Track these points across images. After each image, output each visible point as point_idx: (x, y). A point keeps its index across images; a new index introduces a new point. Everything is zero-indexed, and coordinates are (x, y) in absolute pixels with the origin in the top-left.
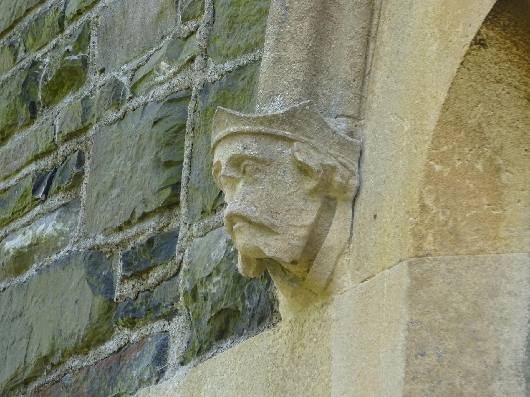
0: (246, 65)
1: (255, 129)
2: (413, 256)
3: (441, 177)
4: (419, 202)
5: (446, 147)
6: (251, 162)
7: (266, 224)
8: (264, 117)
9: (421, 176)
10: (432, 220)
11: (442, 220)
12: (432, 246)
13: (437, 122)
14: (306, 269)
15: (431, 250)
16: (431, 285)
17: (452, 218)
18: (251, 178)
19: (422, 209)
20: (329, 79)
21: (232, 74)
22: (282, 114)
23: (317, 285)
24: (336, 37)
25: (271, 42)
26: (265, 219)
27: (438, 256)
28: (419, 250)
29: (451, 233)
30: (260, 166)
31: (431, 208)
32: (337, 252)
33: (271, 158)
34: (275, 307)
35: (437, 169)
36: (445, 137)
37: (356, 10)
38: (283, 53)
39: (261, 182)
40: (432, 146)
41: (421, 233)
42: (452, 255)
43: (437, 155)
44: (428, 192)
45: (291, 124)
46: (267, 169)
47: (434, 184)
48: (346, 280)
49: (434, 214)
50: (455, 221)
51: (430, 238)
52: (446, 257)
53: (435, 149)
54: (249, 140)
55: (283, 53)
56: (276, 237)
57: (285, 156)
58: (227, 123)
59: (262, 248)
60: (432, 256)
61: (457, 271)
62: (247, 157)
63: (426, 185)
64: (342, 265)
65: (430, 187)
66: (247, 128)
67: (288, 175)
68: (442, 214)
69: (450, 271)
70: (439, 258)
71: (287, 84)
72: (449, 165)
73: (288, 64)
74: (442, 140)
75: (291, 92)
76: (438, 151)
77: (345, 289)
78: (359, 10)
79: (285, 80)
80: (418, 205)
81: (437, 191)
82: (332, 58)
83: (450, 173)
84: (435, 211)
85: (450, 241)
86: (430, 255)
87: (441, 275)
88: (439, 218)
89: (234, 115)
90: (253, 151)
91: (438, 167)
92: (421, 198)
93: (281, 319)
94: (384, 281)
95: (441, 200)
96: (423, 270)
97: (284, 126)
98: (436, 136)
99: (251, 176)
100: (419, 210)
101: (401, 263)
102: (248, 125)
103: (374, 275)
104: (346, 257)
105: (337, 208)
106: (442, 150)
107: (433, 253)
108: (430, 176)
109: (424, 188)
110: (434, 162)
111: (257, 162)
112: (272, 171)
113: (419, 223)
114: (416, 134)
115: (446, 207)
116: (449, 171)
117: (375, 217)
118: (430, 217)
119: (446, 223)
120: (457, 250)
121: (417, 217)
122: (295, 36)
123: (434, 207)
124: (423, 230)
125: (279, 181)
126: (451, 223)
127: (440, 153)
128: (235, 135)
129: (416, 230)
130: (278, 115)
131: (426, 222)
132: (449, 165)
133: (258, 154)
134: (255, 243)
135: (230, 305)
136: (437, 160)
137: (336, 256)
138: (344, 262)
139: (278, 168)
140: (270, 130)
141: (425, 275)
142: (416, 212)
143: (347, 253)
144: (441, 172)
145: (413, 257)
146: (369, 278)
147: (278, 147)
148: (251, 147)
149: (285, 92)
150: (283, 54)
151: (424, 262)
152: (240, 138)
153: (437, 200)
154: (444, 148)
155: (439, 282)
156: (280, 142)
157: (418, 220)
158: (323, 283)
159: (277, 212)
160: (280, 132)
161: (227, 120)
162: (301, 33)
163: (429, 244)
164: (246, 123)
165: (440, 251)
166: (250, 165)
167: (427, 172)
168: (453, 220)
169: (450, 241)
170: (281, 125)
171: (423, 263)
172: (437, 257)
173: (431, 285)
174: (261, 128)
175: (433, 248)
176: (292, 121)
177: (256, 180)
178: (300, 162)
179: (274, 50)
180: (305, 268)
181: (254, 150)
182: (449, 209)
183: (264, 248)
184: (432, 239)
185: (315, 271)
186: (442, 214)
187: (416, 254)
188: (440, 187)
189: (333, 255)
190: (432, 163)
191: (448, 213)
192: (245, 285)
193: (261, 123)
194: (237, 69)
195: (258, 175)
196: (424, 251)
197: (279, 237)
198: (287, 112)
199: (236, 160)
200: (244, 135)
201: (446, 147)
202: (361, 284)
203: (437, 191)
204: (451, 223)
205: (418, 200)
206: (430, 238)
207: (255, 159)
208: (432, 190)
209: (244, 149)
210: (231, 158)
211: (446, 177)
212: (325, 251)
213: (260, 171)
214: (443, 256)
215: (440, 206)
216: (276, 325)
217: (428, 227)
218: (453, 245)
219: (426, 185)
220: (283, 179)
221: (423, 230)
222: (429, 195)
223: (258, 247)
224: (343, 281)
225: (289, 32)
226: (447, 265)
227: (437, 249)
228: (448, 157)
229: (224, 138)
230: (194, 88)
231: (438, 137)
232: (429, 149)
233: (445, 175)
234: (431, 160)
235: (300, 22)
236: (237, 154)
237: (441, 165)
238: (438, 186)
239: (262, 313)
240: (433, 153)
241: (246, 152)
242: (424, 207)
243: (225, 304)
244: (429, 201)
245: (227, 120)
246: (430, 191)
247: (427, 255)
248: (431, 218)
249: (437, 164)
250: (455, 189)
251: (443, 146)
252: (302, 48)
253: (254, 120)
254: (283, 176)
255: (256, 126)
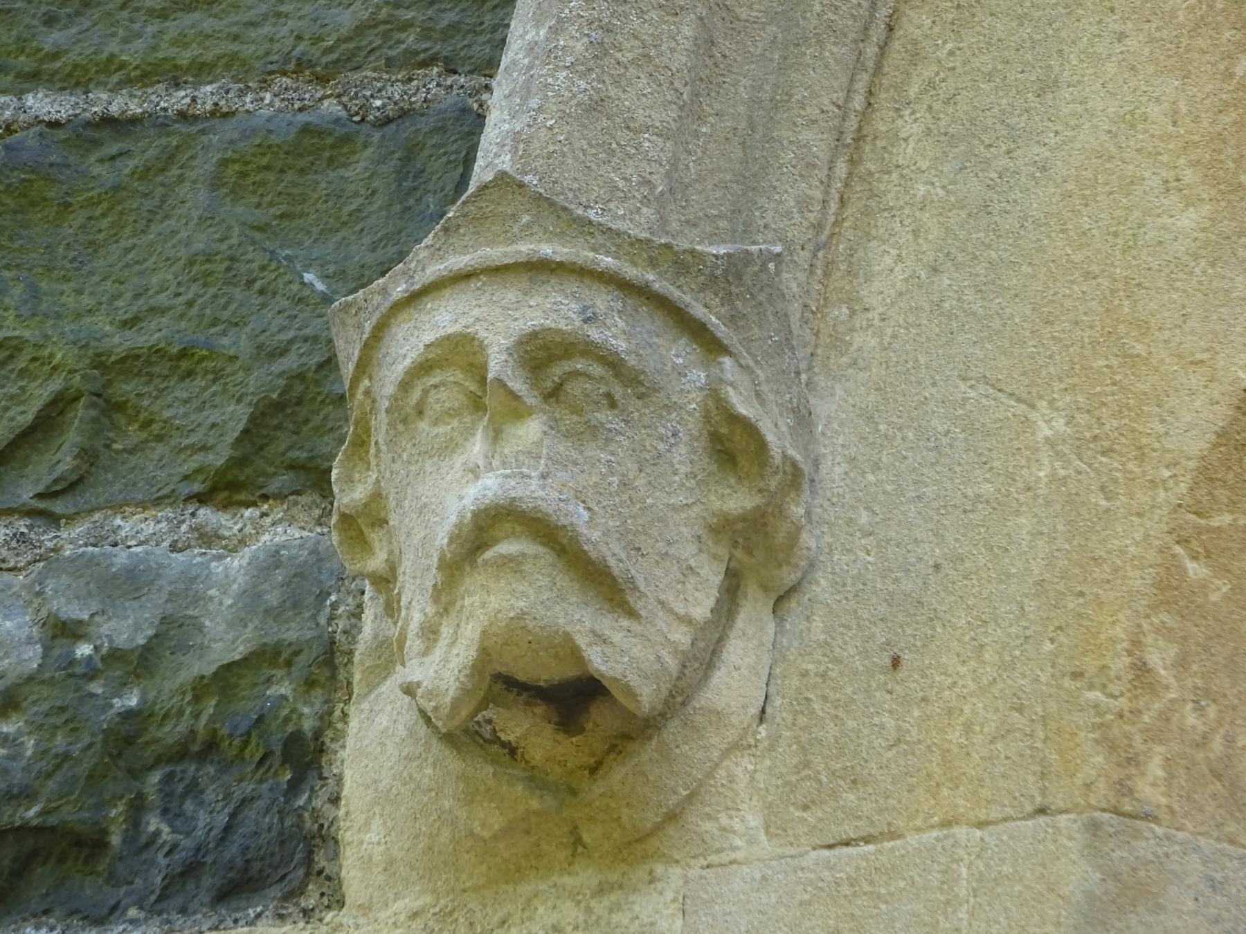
0: (135, 121)
1: (630, 272)
2: (1104, 805)
3: (1200, 601)
4: (1130, 653)
5: (1227, 518)
6: (597, 370)
7: (616, 572)
8: (668, 246)
9: (1139, 581)
10: (1165, 717)
11: (1194, 727)
12: (1163, 794)
13: (1218, 435)
14: (592, 761)
15: (1159, 806)
16: (1160, 908)
17: (1222, 731)
18: (575, 418)
19: (1138, 677)
20: (687, 222)
21: (61, 134)
22: (716, 256)
23: (624, 819)
24: (717, 106)
25: (579, 47)
26: (613, 554)
27: (1177, 829)
28: (1123, 795)
29: (1218, 777)
30: (618, 391)
31: (1165, 682)
32: (731, 735)
33: (658, 378)
34: (320, 860)
35: (1191, 573)
36: (1231, 489)
37: (829, 46)
38: (613, 91)
39: (608, 441)
40: (1188, 500)
41: (1130, 746)
42: (1218, 840)
43: (1199, 533)
44: (1157, 631)
45: (728, 299)
46: (634, 405)
47: (1179, 613)
48: (741, 820)
49: (1172, 701)
50: (1230, 741)
51: (1155, 769)
52: (1202, 841)
53: (1195, 513)
54: (602, 300)
55: (613, 91)
56: (625, 623)
57: (687, 387)
58: (528, 226)
59: (581, 641)
60: (1159, 825)
61: (1234, 891)
62: (590, 350)
63: (1154, 607)
64: (732, 779)
65: (1164, 617)
66: (607, 261)
67: (683, 449)
68: (1195, 709)
69: (1213, 884)
70: (1181, 835)
71: (621, 184)
72: (1228, 571)
73: (628, 128)
74: (1222, 494)
75: (632, 213)
76: (1203, 522)
77: (738, 855)
78: (835, 50)
79: (615, 170)
80: (1127, 660)
81: (1185, 638)
82: (698, 162)
83: (1226, 598)
84: (1172, 695)
85: (1214, 796)
86: (1156, 820)
87: (1189, 887)
88: (1184, 717)
89: (565, 209)
90: (614, 336)
91: (1195, 570)
92: (1136, 643)
93: (341, 904)
94: (958, 861)
95: (1195, 667)
96: (1137, 858)
97: (709, 295)
98: (1205, 475)
99: (577, 410)
100: (1130, 677)
101: (1042, 820)
102: (608, 253)
103: (894, 835)
104: (746, 759)
105: (743, 602)
106: (1215, 523)
107: (1165, 817)
108: (1170, 590)
109: (1148, 616)
110: (1185, 548)
111: (616, 375)
112: (646, 420)
113: (1127, 714)
114: (1104, 453)
115: (1207, 692)
116: (1224, 590)
117: (896, 662)
118: (1157, 706)
119: (1203, 742)
120: (1232, 829)
121: (1122, 695)
122: (653, 52)
123: (1172, 680)
124: (1138, 738)
125: (660, 456)
126: (1217, 744)
127: (1210, 530)
128: (553, 271)
129: (1115, 731)
130: (702, 254)
131: (1146, 718)
132: (1228, 571)
133: (629, 353)
134: (561, 621)
135: (71, 814)
136: (1195, 544)
137: (723, 746)
138: (739, 771)
139: (661, 417)
140: (674, 293)
141: (1142, 874)
142: (1119, 678)
143: (750, 746)
144: (1204, 586)
145: (1104, 810)
146: (867, 840)
147: (678, 352)
148: (608, 322)
149: (612, 206)
150: (612, 94)
151: (1137, 834)
152: (573, 285)
153: (1181, 664)
154: (1223, 520)
155: (1184, 908)
156: (683, 341)
157: (1123, 703)
158: (652, 818)
159: (639, 549)
160: (698, 311)
161: (526, 219)
162: (672, 51)
163: (1154, 785)
164: (604, 245)
165: (1185, 816)
166: (589, 377)
167: (1162, 570)
168: (1225, 737)
169: (1214, 796)
170: (703, 288)
171: (1136, 838)
172: (1173, 832)
173: (1160, 908)
174: (651, 277)
175: (1163, 800)
176: (733, 288)
177: (594, 430)
178: (735, 419)
179: (590, 70)
180: (592, 755)
181: (617, 330)
182: (1214, 701)
183: (590, 645)
184: (1160, 773)
185: (644, 774)
186: (1195, 709)
187: (1113, 801)
188: (1195, 629)
189: (715, 740)
190: (1178, 550)
191: (1212, 711)
192: (152, 767)
193: (653, 263)
194: (88, 124)
195: (603, 416)
196: (1137, 800)
197: (636, 627)
198: (729, 255)
199: (545, 347)
200: (587, 281)
201: (1227, 518)
202: (826, 853)
203: (1185, 638)
204: (1217, 744)
205: (1126, 645)
206: (1155, 769)
207: (613, 363)
208: (1170, 630)
209: (587, 320)
210: (534, 335)
211: (1215, 604)
212: (698, 718)
213: (613, 404)
214: (1192, 833)
215: (1189, 683)
216: (317, 914)
217: (1154, 736)
218: (1223, 811)
219: (1154, 607)
220: (668, 455)
221: (1138, 738)
222: (1161, 643)
223: (566, 634)
224: (724, 829)
225: (636, 38)
226: (1205, 863)
227: (1176, 807)
228: (1229, 549)
229: (497, 271)
230: (52, 39)
231: (1211, 479)
232: (1180, 506)
233: (1214, 597)
234: (1178, 542)
235: (672, 19)
236: (558, 331)
237: (1207, 565)
238: (1188, 624)
239: (246, 870)
240: (1187, 522)
241: (594, 334)
242: (1142, 670)
243: (44, 813)
244: (1159, 657)
245: (526, 219)
246: (1163, 631)
247: (1147, 817)
248: (1161, 713)
249: (1195, 558)
250: (1236, 648)
251: (1220, 510)
252: (669, 97)
253: (631, 245)
254: (672, 445)
255: (634, 264)
